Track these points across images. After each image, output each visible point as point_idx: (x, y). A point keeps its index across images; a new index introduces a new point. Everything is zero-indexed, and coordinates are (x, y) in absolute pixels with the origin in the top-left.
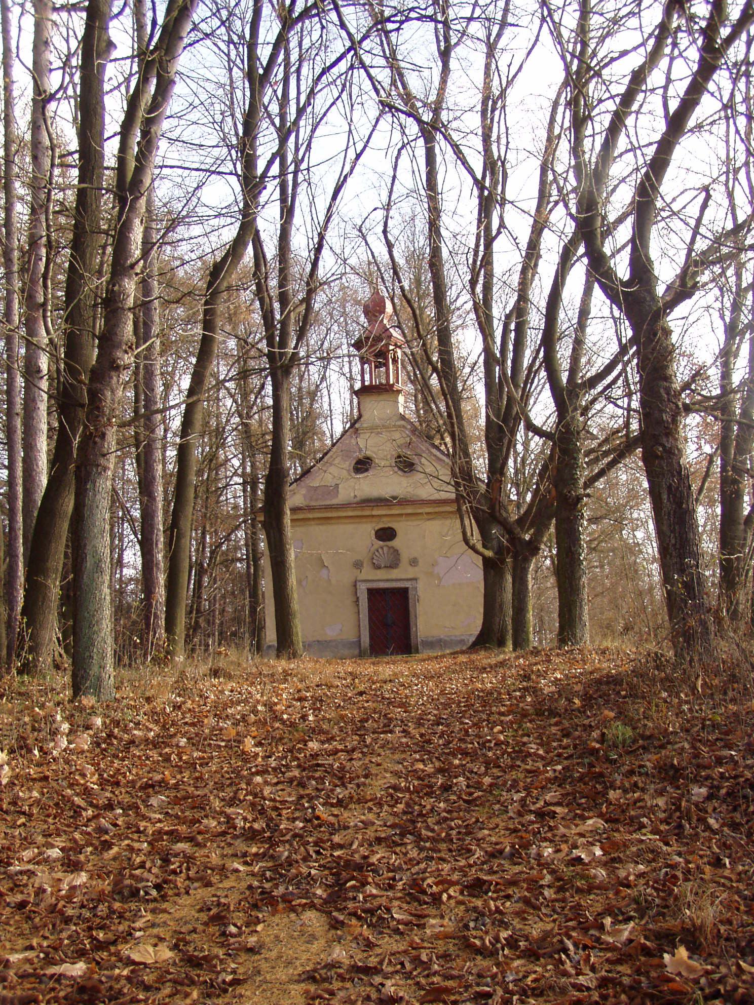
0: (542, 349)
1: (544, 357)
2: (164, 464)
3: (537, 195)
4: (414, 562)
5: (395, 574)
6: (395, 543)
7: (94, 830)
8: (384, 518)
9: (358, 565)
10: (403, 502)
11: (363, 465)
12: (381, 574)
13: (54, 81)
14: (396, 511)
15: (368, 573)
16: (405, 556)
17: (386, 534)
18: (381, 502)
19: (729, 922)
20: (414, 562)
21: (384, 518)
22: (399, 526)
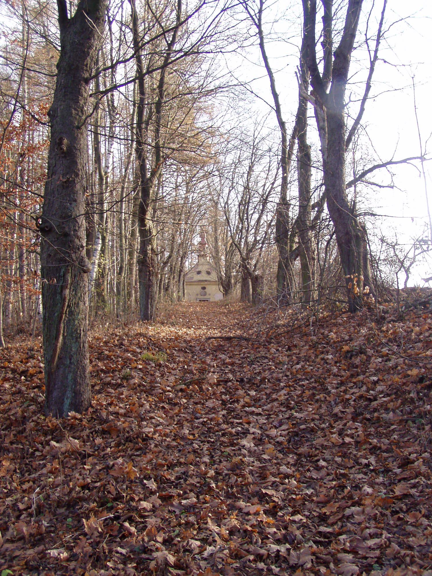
0: (296, 141)
1: (300, 147)
2: (319, 261)
3: (265, 44)
4: (210, 295)
5: (205, 297)
6: (206, 290)
7: (175, 479)
8: (203, 284)
9: (197, 295)
10: (206, 281)
11: (199, 273)
12: (202, 297)
13: (115, 165)
14: (206, 283)
15: (199, 297)
16: (208, 293)
17: (204, 288)
18: (202, 281)
19: (381, 457)
20: (210, 295)
21: (203, 284)
22: (207, 287)
